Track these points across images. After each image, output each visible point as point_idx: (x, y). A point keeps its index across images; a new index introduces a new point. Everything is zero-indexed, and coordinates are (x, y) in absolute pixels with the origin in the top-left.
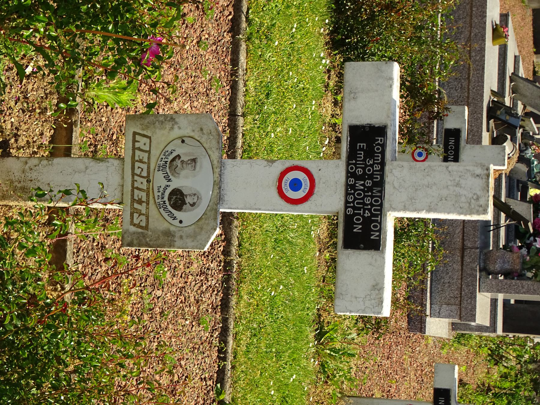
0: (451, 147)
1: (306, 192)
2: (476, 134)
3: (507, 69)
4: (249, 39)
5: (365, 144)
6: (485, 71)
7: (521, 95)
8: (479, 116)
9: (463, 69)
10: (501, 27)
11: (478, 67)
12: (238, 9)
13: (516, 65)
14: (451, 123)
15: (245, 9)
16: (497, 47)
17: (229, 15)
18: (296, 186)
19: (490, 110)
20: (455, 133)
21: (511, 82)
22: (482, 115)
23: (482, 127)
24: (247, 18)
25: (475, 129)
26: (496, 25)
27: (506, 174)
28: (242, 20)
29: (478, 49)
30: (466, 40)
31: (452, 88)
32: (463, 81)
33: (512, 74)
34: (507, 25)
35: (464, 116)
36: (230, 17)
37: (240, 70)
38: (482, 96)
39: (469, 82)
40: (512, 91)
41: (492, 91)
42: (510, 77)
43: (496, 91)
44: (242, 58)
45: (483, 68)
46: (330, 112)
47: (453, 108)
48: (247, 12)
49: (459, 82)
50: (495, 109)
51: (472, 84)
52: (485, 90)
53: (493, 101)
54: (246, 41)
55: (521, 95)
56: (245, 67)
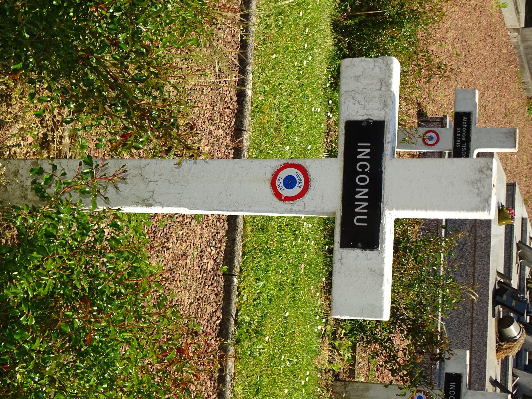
0: (363, 167)
1: (302, 187)
2: (481, 323)
3: (514, 238)
4: (238, 342)
5: (364, 140)
6: (491, 258)
7: (528, 261)
8: (485, 304)
9: (468, 255)
10: (507, 209)
11: (484, 255)
12: (226, 312)
13: (523, 228)
14: (451, 368)
15: (233, 312)
16: (503, 227)
17: (217, 320)
18: (290, 183)
19: (496, 292)
20: (456, 378)
21: (518, 250)
22: (488, 303)
23: (487, 316)
24: (236, 321)
25: (481, 318)
26: (502, 206)
27: (513, 356)
28: (231, 324)
29: (483, 236)
30: (471, 226)
31: (457, 274)
32: (468, 267)
33: (519, 242)
34: (513, 208)
35: (465, 361)
36: (219, 322)
37: (228, 376)
38: (488, 284)
39: (474, 269)
40: (519, 257)
41: (498, 272)
42: (517, 244)
43: (503, 273)
44: (230, 364)
45: (489, 256)
46: (327, 358)
47: (455, 351)
48: (237, 315)
49: (464, 269)
50: (503, 289)
51: (477, 271)
52: (490, 278)
53: (499, 282)
54: (234, 346)
55: (528, 261)
56: (233, 372)
